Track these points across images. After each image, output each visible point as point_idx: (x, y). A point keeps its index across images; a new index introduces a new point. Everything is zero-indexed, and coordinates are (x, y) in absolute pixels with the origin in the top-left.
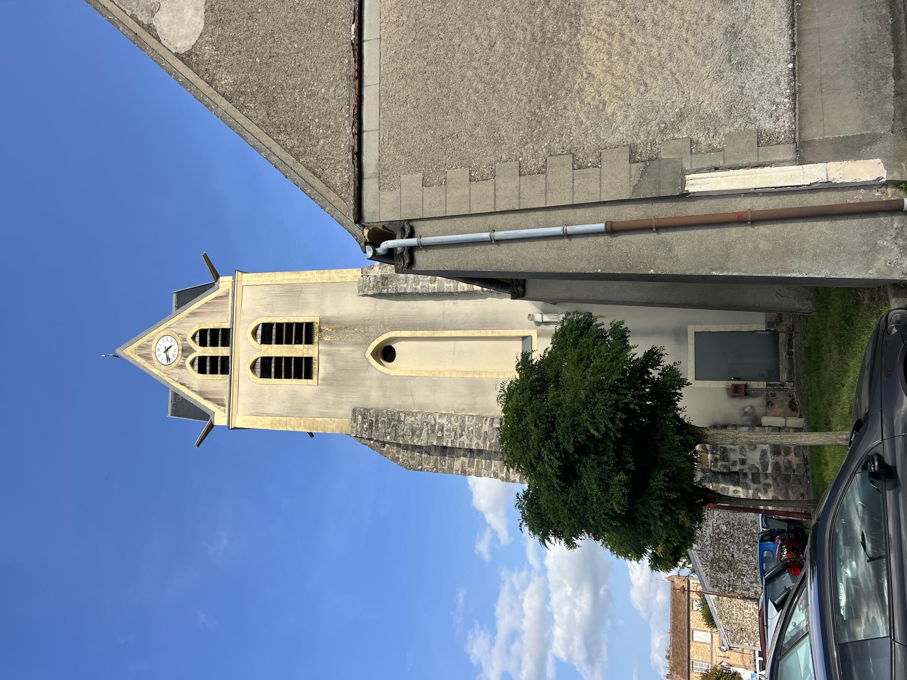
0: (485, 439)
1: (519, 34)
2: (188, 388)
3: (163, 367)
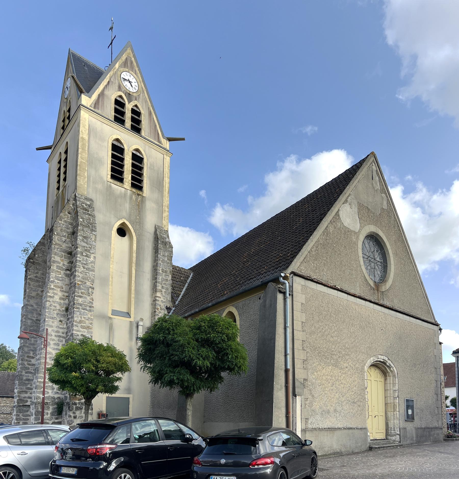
0: (82, 282)
1: (334, 347)
2: (106, 86)
3: (119, 73)
